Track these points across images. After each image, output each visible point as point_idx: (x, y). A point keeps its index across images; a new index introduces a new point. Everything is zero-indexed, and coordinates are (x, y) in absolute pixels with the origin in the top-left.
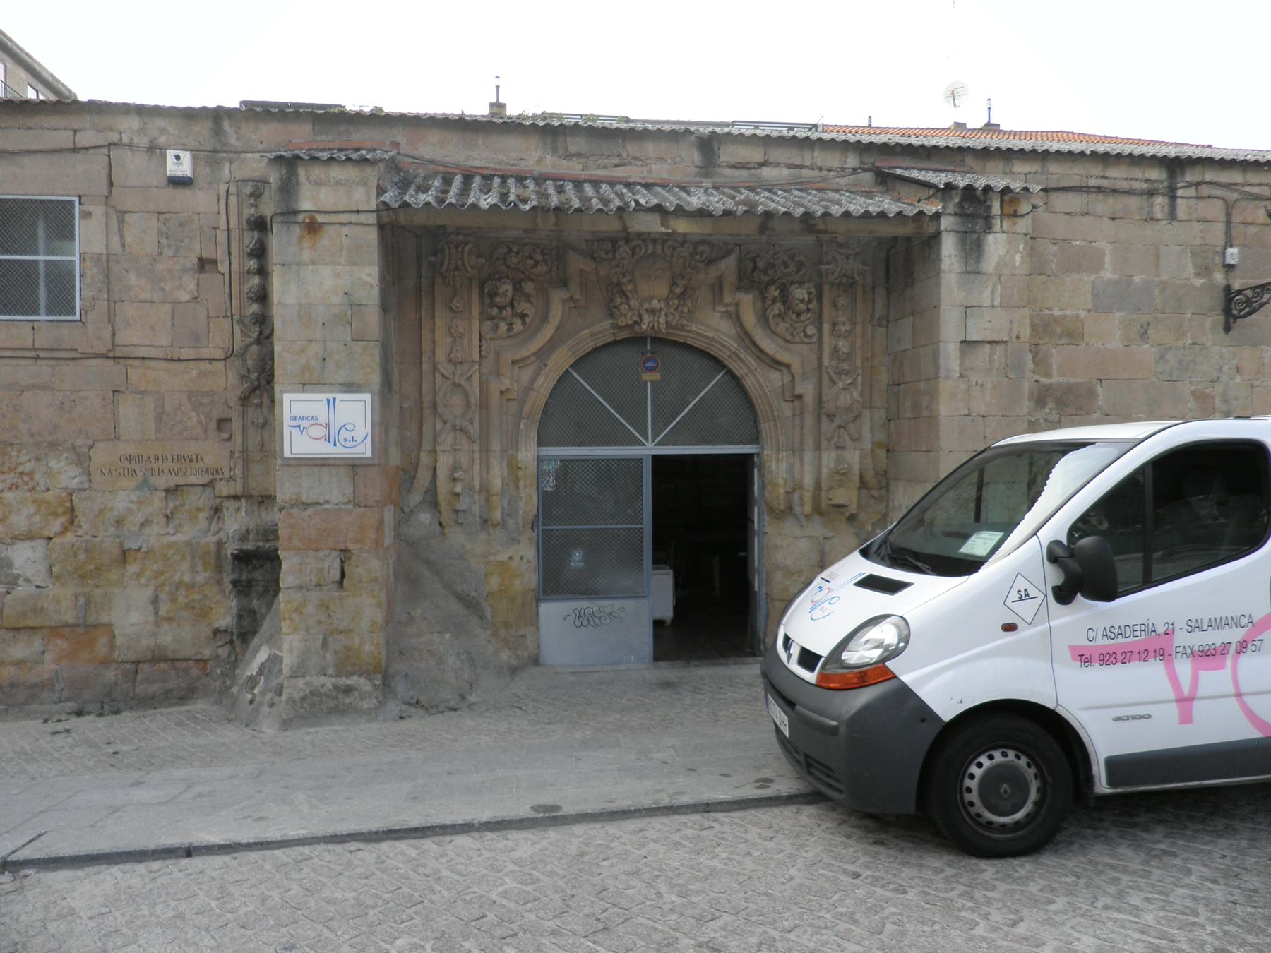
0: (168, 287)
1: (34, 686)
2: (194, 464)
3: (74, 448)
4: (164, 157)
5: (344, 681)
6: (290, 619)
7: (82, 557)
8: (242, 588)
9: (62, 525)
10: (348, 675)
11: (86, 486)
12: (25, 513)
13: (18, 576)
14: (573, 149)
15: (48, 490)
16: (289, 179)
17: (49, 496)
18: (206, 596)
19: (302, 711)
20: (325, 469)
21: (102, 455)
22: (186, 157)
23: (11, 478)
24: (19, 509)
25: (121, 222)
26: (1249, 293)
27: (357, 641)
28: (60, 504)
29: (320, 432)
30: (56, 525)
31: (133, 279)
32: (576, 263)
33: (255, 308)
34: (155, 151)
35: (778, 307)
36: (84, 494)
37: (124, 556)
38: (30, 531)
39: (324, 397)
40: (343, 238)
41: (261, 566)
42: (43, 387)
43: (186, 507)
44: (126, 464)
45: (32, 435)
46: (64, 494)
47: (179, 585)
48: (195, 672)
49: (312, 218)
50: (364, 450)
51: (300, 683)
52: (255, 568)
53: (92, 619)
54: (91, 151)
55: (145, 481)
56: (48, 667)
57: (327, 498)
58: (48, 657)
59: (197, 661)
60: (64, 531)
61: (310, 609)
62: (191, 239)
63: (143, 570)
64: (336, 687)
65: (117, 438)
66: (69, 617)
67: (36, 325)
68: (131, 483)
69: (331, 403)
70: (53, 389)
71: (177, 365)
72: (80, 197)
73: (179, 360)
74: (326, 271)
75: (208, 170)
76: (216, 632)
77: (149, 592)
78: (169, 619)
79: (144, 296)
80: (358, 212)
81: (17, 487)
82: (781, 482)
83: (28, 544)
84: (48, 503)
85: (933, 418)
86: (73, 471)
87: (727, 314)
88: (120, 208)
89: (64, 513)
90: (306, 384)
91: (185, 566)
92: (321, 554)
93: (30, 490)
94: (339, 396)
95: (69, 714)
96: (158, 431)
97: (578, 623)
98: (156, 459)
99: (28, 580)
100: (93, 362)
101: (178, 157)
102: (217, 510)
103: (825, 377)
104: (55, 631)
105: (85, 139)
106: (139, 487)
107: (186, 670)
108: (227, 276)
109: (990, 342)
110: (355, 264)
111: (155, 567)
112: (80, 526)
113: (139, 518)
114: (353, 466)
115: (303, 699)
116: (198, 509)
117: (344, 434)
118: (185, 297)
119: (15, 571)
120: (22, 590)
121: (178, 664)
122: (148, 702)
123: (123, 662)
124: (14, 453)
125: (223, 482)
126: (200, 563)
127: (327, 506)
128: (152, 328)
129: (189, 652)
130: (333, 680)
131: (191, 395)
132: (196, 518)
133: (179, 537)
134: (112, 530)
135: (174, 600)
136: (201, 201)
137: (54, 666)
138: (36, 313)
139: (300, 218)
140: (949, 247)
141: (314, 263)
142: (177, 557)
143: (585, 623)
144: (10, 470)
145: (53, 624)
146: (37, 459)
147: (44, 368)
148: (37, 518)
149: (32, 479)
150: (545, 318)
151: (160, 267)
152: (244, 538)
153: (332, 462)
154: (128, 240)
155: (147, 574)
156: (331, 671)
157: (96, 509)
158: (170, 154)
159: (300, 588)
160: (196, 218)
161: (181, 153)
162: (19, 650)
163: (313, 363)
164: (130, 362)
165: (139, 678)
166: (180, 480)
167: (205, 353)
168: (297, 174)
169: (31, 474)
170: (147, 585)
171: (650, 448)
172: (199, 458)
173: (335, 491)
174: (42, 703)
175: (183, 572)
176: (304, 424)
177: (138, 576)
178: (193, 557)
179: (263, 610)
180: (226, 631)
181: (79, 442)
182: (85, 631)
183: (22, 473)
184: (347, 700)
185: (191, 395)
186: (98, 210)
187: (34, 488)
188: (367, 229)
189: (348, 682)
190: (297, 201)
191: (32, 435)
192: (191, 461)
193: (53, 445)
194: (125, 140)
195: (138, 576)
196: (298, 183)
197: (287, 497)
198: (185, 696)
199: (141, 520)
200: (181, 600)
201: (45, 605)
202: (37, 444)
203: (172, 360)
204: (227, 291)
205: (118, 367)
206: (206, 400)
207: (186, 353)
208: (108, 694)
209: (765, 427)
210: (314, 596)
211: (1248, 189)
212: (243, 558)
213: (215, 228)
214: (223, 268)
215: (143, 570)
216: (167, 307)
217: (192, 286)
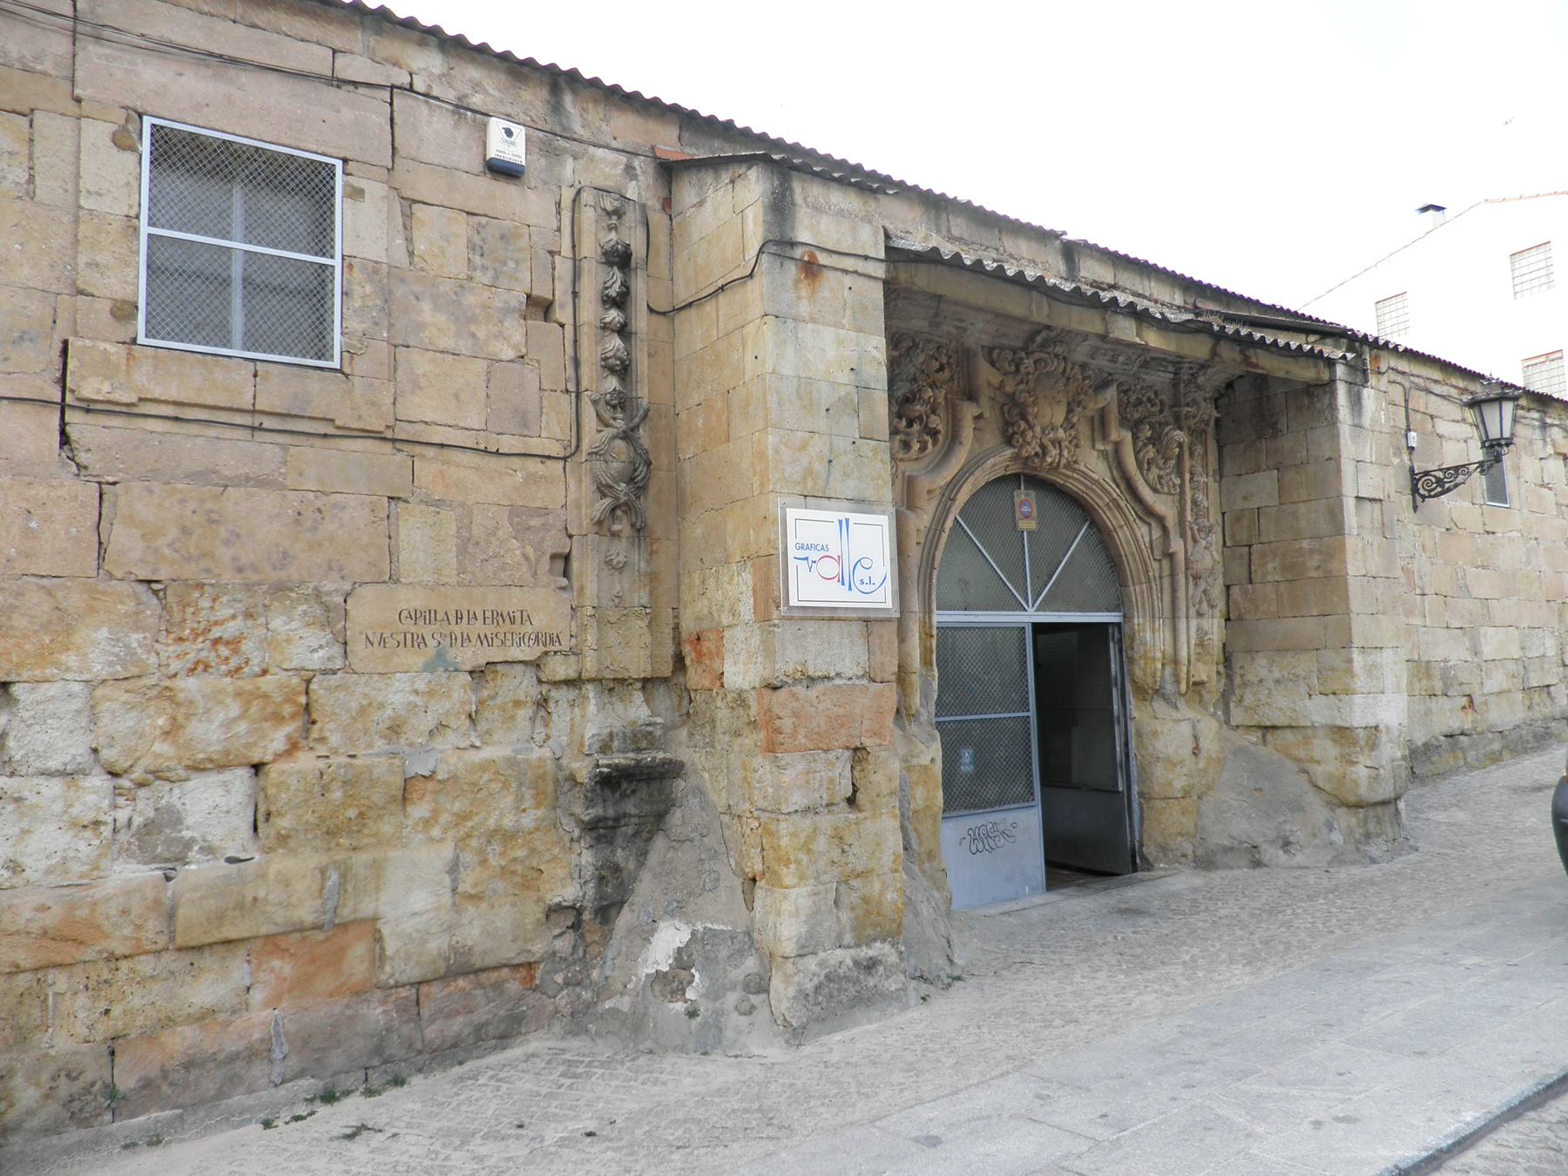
0: (481, 333)
1: (233, 1058)
2: (517, 628)
3: (318, 594)
4: (483, 129)
5: (866, 952)
6: (798, 862)
7: (337, 795)
8: (600, 831)
9: (288, 737)
10: (869, 942)
11: (338, 664)
12: (220, 716)
13: (188, 844)
14: (956, 232)
15: (265, 672)
16: (783, 194)
17: (266, 683)
18: (533, 851)
19: (817, 1009)
20: (833, 624)
21: (368, 611)
22: (520, 132)
23: (198, 649)
24: (207, 711)
25: (408, 216)
26: (1440, 475)
27: (877, 886)
28: (288, 700)
29: (830, 568)
30: (277, 740)
31: (426, 312)
32: (986, 374)
33: (612, 383)
34: (468, 114)
35: (1151, 452)
36: (333, 680)
37: (406, 793)
38: (227, 753)
39: (836, 516)
40: (846, 292)
41: (634, 792)
42: (264, 483)
43: (499, 701)
44: (408, 625)
45: (240, 570)
46: (295, 681)
47: (491, 836)
48: (514, 987)
49: (812, 255)
50: (882, 597)
51: (811, 963)
52: (624, 796)
53: (346, 913)
54: (361, 90)
55: (440, 655)
56: (260, 1017)
57: (838, 669)
58: (257, 996)
59: (515, 967)
60: (293, 748)
61: (821, 844)
62: (517, 262)
63: (435, 813)
64: (856, 963)
65: (394, 579)
66: (306, 913)
67: (260, 366)
68: (416, 659)
69: (844, 525)
70: (283, 487)
71: (493, 462)
72: (345, 161)
73: (497, 453)
74: (828, 334)
75: (543, 161)
76: (554, 911)
77: (447, 850)
78: (475, 898)
79: (446, 342)
80: (866, 258)
81: (207, 667)
82: (1159, 655)
83: (213, 778)
84: (266, 696)
85: (1344, 578)
86: (315, 637)
87: (1104, 454)
88: (408, 193)
89: (293, 716)
90: (813, 496)
91: (508, 801)
92: (831, 756)
93: (230, 673)
94: (855, 517)
95: (311, 1101)
96: (462, 570)
97: (974, 849)
98: (459, 618)
99: (209, 850)
100: (358, 444)
101: (509, 133)
102: (543, 703)
103: (1189, 533)
104: (272, 943)
105: (354, 67)
106: (430, 667)
107: (498, 986)
108: (569, 329)
109: (1370, 500)
110: (860, 330)
111: (457, 806)
112: (322, 740)
113: (429, 721)
114: (867, 621)
115: (818, 988)
116: (517, 704)
117: (860, 574)
118: (509, 354)
119: (187, 834)
120: (197, 869)
121: (483, 977)
122: (447, 1053)
123: (397, 986)
124: (205, 603)
125: (559, 657)
126: (528, 793)
127: (838, 682)
128: (456, 397)
129: (509, 953)
130: (852, 952)
131: (514, 511)
132: (513, 718)
133: (487, 753)
134: (380, 744)
135: (483, 862)
136: (529, 207)
137: (267, 1014)
138: (227, 343)
139: (798, 252)
140: (1342, 390)
141: (813, 320)
142: (495, 786)
143: (980, 847)
144: (196, 635)
145: (273, 929)
146: (249, 615)
147: (268, 451)
148: (242, 727)
149: (236, 652)
150: (954, 437)
151: (471, 299)
152: (605, 748)
153: (842, 615)
154: (420, 247)
155: (445, 818)
156: (848, 938)
157: (354, 705)
158: (496, 126)
159: (807, 810)
160: (526, 230)
161: (515, 128)
162: (208, 988)
163: (817, 466)
164: (418, 449)
165: (425, 1012)
166: (496, 655)
167: (536, 445)
168: (790, 189)
169: (234, 643)
170: (442, 840)
171: (1032, 615)
172: (525, 618)
173: (844, 656)
174: (250, 1091)
175: (503, 812)
176: (813, 555)
177: (427, 823)
178: (521, 784)
179: (631, 866)
180: (573, 907)
181: (328, 586)
182: (329, 936)
183: (216, 642)
184: (871, 982)
185: (514, 511)
186: (375, 190)
187: (238, 669)
188: (872, 283)
189: (871, 953)
190: (793, 228)
191: (240, 570)
192: (513, 622)
193: (280, 589)
194: (419, 86)
195: (427, 823)
196: (793, 203)
197: (790, 669)
198: (507, 1032)
199: (432, 725)
200: (495, 861)
201: (261, 894)
202: (249, 587)
203: (486, 451)
204: (570, 351)
205: (400, 456)
206: (536, 522)
207: (508, 444)
208: (378, 1050)
209: (1136, 591)
210: (826, 821)
211: (1416, 380)
212: (611, 782)
213: (551, 253)
214: (563, 314)
215: (435, 813)
216: (481, 365)
217: (518, 337)
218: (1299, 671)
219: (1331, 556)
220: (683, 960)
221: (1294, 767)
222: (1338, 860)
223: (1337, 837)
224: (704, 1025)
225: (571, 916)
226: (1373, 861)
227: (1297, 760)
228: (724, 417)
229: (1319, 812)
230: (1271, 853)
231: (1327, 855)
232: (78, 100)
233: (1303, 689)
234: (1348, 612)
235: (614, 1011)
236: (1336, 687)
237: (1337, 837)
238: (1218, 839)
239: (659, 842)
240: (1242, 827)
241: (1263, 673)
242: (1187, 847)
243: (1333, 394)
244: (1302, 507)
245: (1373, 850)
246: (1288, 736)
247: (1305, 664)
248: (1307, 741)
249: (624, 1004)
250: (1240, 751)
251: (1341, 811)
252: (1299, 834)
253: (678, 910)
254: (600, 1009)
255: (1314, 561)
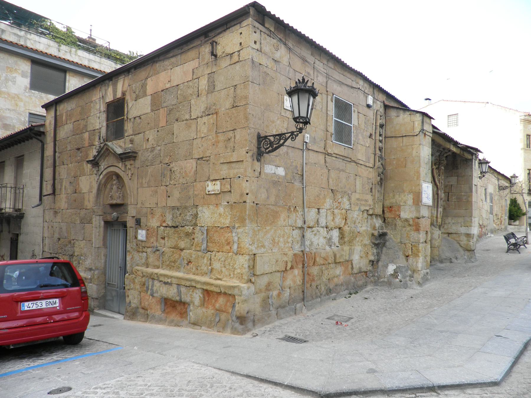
34: (366, 95)
167: (367, 164)
218: (459, 221)
219: (469, 197)
220: (396, 272)
221: (456, 242)
222: (466, 262)
223: (466, 257)
224: (404, 283)
225: (372, 262)
226: (473, 262)
227: (457, 241)
228: (404, 163)
229: (462, 252)
230: (454, 260)
231: (464, 261)
232: (327, 91)
233: (460, 225)
234: (472, 209)
235: (383, 281)
236: (468, 225)
237: (466, 257)
238: (443, 257)
239: (384, 249)
240: (448, 254)
241: (450, 221)
242: (438, 259)
243: (472, 161)
244: (463, 186)
245: (473, 260)
246: (455, 235)
247: (461, 220)
248: (459, 236)
249: (386, 280)
250: (444, 238)
251: (466, 252)
252: (459, 257)
253: (392, 262)
254: (380, 281)
255: (465, 197)
